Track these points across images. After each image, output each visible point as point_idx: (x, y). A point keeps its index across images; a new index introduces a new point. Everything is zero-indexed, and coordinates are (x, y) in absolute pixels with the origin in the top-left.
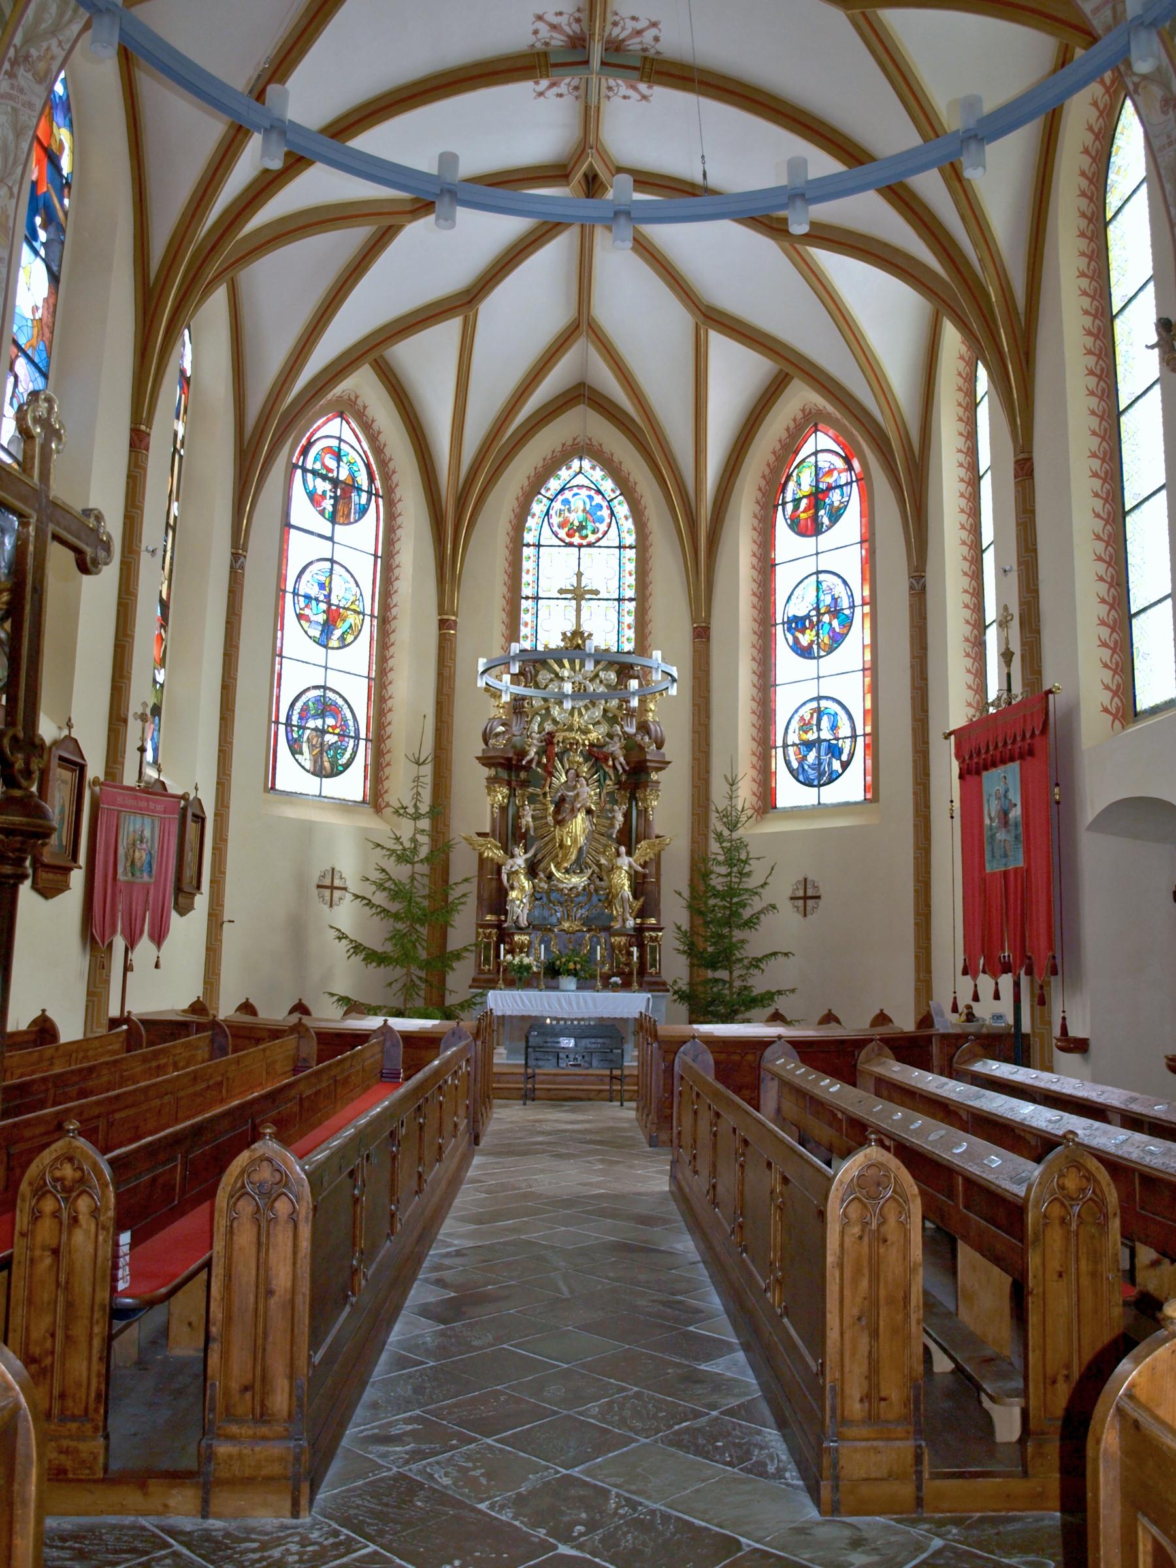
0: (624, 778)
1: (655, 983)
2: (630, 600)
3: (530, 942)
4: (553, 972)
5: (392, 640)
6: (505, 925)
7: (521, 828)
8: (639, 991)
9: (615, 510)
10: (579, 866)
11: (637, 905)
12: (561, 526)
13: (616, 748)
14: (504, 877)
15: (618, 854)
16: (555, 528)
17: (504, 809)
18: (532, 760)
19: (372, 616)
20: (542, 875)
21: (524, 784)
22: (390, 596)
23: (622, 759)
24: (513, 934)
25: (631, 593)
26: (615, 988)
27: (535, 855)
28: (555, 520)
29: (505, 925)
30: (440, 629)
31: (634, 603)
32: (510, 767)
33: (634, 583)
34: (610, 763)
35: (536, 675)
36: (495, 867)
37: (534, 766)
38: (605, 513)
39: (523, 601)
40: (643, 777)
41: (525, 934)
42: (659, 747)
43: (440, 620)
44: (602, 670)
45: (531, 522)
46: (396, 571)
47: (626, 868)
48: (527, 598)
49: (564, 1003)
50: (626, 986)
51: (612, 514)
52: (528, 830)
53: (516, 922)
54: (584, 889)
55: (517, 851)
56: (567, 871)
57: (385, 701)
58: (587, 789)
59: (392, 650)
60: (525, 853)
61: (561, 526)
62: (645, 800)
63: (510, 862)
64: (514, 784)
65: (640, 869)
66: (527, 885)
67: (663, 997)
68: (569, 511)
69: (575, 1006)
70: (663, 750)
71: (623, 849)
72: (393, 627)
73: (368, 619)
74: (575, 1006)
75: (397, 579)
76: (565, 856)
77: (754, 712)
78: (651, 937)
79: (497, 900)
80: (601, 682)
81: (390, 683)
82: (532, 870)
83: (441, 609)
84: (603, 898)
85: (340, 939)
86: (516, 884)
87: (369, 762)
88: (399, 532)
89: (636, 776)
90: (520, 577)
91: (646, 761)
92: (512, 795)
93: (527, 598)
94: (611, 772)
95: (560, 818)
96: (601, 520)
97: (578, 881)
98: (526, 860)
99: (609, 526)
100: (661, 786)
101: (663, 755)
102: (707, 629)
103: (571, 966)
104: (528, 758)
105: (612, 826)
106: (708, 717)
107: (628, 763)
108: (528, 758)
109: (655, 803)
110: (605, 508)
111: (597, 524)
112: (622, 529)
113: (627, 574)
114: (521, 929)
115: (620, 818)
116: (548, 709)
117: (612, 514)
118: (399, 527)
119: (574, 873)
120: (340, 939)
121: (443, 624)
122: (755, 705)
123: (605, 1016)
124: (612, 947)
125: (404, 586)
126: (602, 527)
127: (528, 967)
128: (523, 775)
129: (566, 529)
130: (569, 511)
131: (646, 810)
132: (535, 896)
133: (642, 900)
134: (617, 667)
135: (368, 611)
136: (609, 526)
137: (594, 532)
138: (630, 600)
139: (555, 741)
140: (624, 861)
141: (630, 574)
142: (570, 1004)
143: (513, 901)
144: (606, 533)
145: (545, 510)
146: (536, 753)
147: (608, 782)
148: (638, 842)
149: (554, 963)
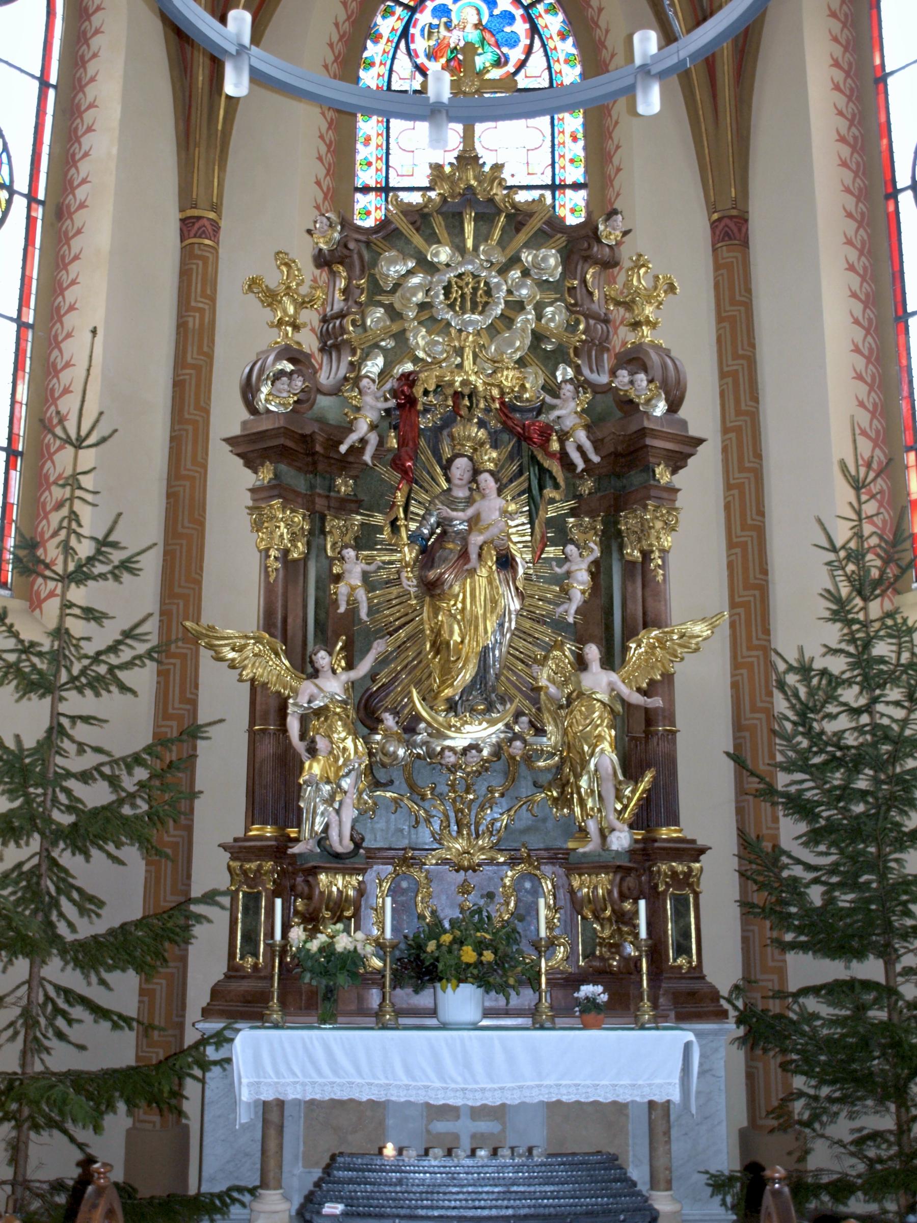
0: (587, 486)
1: (692, 995)
2: (576, 186)
3: (361, 891)
4: (419, 967)
5: (75, 250)
6: (296, 849)
7: (335, 603)
8: (657, 1022)
9: (540, 22)
10: (483, 695)
11: (635, 793)
12: (432, 55)
13: (568, 412)
14: (293, 726)
15: (581, 664)
16: (422, 60)
17: (292, 568)
18: (363, 441)
19: (31, 198)
20: (389, 720)
21: (347, 505)
22: (75, 164)
23: (582, 436)
24: (314, 871)
25: (576, 174)
26: (590, 1015)
27: (372, 676)
28: (420, 45)
29: (296, 849)
30: (183, 238)
31: (583, 193)
32: (301, 456)
33: (582, 154)
34: (555, 446)
35: (374, 263)
36: (273, 704)
37: (367, 457)
38: (520, 27)
39: (358, 196)
40: (636, 478)
41: (345, 872)
42: (674, 406)
43: (183, 221)
44: (527, 245)
45: (373, 50)
46: (88, 117)
47: (605, 697)
48: (366, 190)
49: (448, 1062)
50: (621, 1006)
51: (534, 30)
52: (353, 611)
53: (322, 840)
54: (498, 751)
55: (322, 658)
56: (452, 706)
57: (57, 373)
58: (499, 502)
59: (74, 268)
60: (350, 666)
61: (432, 55)
62: (644, 530)
63: (307, 688)
64: (320, 503)
65: (637, 699)
66: (350, 745)
67: (716, 1033)
68: (448, 26)
69: (479, 1068)
70: (682, 413)
71: (593, 652)
72: (78, 223)
73: (20, 203)
74: (479, 1068)
75: (90, 129)
76: (447, 672)
77: (859, 377)
78: (675, 874)
79: (275, 786)
80: (526, 273)
81: (69, 335)
82: (366, 712)
83: (186, 198)
84: (545, 779)
85: (457, 871)
86: (321, 744)
87: (14, 498)
88: (96, 42)
89: (624, 470)
90: (353, 151)
91: (643, 432)
92: (318, 531)
93: (366, 190)
94: (555, 468)
95: (432, 575)
96: (513, 42)
97: (477, 733)
98: (352, 685)
99: (529, 51)
100: (681, 500)
101: (684, 424)
102: (742, 220)
103: (468, 955)
104: (353, 438)
105: (565, 592)
106: (755, 398)
107: (597, 445)
108: (353, 438)
109: (667, 541)
110: (519, 20)
111: (505, 50)
112: (553, 55)
113: (568, 140)
114: (337, 856)
115: (581, 580)
116: (401, 337)
117: (534, 30)
118: (97, 32)
119: (472, 710)
120: (457, 871)
121: (189, 226)
122: (860, 363)
123: (568, 1097)
124: (577, 904)
125: (103, 145)
126: (516, 54)
127: (353, 959)
128: (344, 486)
129: (443, 61)
130: (448, 26)
131: (646, 555)
132: (376, 774)
133: (648, 777)
134: (562, 240)
135: (21, 184)
136: (529, 51)
137: (498, 64)
138: (576, 186)
139: (418, 391)
140: (599, 681)
141: (575, 139)
142: (467, 1065)
143: (313, 782)
144: (522, 64)
145: (400, 26)
146: (373, 427)
147: (549, 493)
148: (630, 633)
149: (420, 947)
